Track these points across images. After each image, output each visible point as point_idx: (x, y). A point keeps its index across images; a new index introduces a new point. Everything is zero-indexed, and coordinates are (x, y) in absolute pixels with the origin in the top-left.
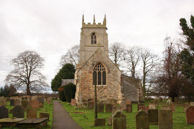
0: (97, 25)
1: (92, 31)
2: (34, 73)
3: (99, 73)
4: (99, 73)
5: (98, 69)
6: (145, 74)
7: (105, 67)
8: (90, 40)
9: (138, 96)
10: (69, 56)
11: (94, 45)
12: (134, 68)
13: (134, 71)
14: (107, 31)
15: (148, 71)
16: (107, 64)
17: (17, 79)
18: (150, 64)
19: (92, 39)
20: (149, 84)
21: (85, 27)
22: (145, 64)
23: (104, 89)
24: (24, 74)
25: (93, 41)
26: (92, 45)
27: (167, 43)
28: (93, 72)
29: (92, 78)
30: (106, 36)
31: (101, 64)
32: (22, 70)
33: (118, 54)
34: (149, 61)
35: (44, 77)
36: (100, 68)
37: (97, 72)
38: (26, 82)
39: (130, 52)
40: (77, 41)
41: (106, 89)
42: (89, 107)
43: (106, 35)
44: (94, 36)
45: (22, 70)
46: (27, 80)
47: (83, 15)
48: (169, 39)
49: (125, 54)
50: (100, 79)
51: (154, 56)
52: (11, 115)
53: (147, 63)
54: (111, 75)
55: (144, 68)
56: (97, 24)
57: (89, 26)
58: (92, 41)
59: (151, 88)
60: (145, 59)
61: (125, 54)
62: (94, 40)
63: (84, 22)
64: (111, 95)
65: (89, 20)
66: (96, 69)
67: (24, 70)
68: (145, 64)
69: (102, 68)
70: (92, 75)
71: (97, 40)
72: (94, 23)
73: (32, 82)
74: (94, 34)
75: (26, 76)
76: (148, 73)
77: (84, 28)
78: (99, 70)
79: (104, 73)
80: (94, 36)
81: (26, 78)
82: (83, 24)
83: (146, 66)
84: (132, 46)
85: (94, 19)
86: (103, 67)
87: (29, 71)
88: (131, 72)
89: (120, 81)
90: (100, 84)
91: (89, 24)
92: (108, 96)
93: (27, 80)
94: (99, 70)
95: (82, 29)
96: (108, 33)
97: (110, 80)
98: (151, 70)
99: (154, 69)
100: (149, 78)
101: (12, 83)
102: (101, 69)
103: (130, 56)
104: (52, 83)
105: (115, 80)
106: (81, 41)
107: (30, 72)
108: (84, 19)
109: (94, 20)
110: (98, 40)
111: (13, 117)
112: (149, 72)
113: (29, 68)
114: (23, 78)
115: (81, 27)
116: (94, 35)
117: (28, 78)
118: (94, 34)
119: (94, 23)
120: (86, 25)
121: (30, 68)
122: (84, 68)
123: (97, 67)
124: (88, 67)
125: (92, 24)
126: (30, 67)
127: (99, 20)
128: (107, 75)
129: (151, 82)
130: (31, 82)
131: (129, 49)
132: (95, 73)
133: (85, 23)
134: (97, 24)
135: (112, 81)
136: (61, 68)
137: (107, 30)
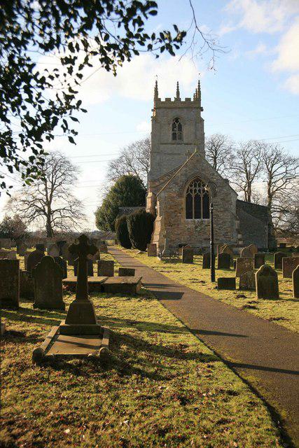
1: (172, 114)
2: (60, 194)
3: (197, 197)
4: (197, 197)
5: (195, 191)
6: (271, 196)
8: (171, 132)
9: (267, 238)
10: (125, 162)
11: (178, 141)
12: (249, 184)
13: (250, 191)
14: (203, 115)
15: (277, 190)
17: (26, 206)
18: (282, 176)
19: (174, 126)
20: (278, 215)
21: (161, 107)
22: (271, 177)
24: (40, 196)
28: (185, 194)
29: (184, 206)
32: (37, 188)
33: (219, 157)
34: (279, 170)
35: (77, 202)
37: (193, 195)
38: (44, 211)
39: (244, 153)
40: (143, 129)
43: (202, 121)
45: (37, 188)
46: (46, 208)
49: (233, 157)
50: (197, 207)
51: (290, 160)
52: (116, 275)
53: (276, 173)
55: (270, 184)
56: (183, 100)
58: (174, 135)
59: (281, 223)
60: (272, 167)
61: (233, 157)
65: (167, 93)
66: (191, 191)
67: (41, 190)
68: (271, 177)
70: (184, 200)
72: (178, 99)
73: (56, 210)
74: (177, 120)
75: (45, 201)
76: (278, 193)
79: (206, 197)
81: (45, 203)
82: (157, 99)
83: (273, 181)
84: (246, 141)
85: (178, 90)
87: (49, 191)
88: (244, 192)
89: (234, 212)
90: (197, 216)
93: (46, 208)
98: (282, 187)
99: (289, 186)
100: (278, 203)
101: (18, 212)
102: (199, 191)
103: (241, 161)
104: (97, 214)
105: (226, 210)
106: (153, 134)
107: (52, 192)
109: (178, 93)
110: (185, 130)
112: (278, 192)
113: (49, 185)
114: (39, 205)
115: (152, 106)
117: (48, 204)
118: (177, 120)
119: (178, 99)
121: (51, 184)
125: (173, 100)
126: (52, 182)
127: (187, 93)
128: (212, 200)
129: (283, 211)
130: (54, 211)
131: (239, 147)
132: (189, 197)
134: (183, 100)
136: (114, 184)
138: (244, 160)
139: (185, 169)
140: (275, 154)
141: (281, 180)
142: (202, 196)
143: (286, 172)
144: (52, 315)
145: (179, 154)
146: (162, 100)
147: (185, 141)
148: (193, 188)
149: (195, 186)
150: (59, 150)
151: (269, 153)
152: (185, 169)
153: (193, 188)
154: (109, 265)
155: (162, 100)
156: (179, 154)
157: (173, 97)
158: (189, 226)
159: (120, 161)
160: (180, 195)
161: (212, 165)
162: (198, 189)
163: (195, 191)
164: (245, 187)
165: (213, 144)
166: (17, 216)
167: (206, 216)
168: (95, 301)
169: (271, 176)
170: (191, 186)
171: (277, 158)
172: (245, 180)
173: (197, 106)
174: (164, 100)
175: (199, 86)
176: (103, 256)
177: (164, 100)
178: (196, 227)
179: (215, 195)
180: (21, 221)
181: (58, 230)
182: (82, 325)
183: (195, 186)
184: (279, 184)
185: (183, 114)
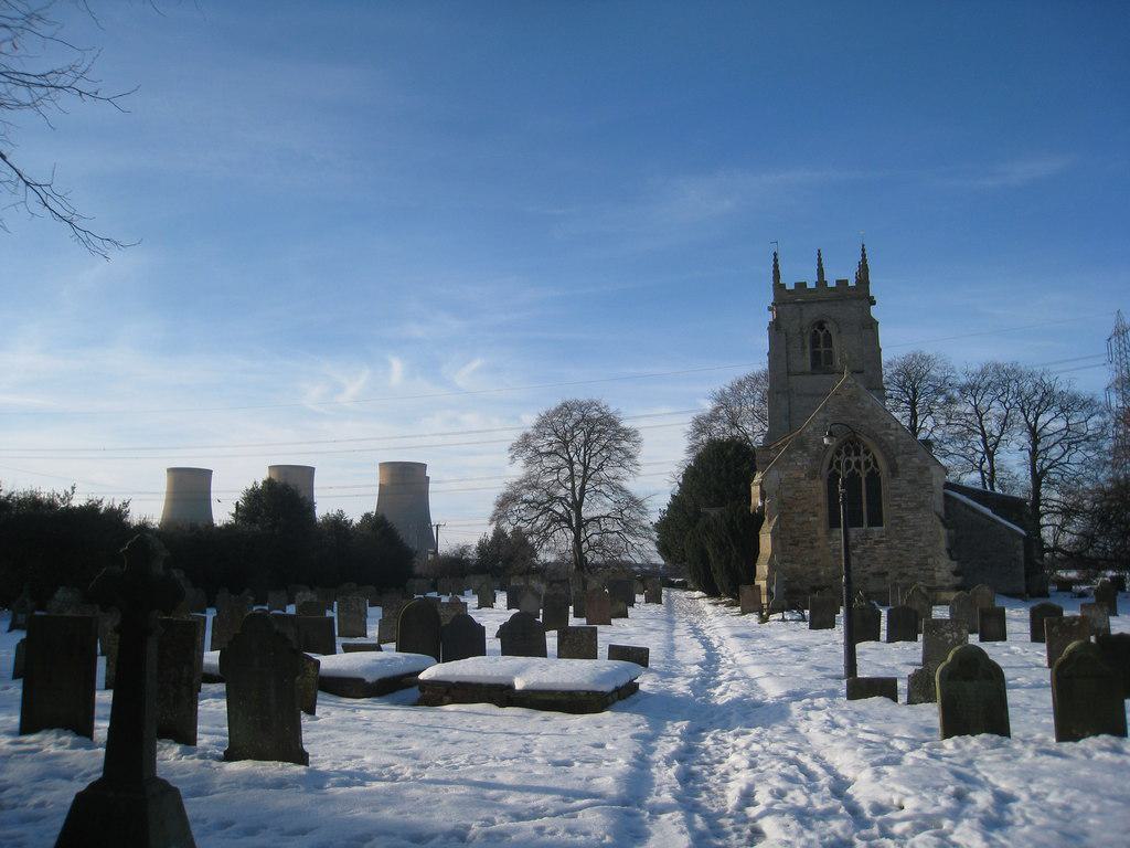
1: (812, 313)
3: (852, 481)
6: (1037, 477)
12: (990, 454)
14: (875, 312)
15: (1050, 467)
16: (885, 438)
18: (1057, 437)
19: (815, 342)
21: (787, 301)
23: (877, 542)
24: (562, 492)
29: (822, 498)
38: (569, 521)
44: (821, 334)
55: (1034, 454)
56: (832, 284)
58: (816, 356)
60: (1036, 419)
62: (822, 349)
64: (905, 570)
65: (798, 273)
66: (838, 463)
72: (821, 282)
74: (821, 325)
79: (874, 478)
82: (778, 286)
83: (1040, 447)
88: (979, 474)
90: (854, 520)
91: (801, 286)
98: (1062, 461)
103: (969, 409)
105: (922, 505)
106: (773, 356)
109: (820, 272)
114: (560, 509)
116: (822, 328)
117: (577, 505)
118: (821, 325)
119: (821, 282)
122: (791, 460)
125: (852, 283)
126: (584, 464)
127: (841, 271)
130: (588, 521)
131: (963, 380)
134: (832, 284)
138: (976, 406)
139: (822, 415)
140: (1040, 391)
141: (1058, 447)
142: (863, 476)
143: (1068, 428)
148: (843, 459)
150: (595, 398)
151: (1028, 386)
152: (822, 415)
153: (843, 459)
154: (586, 636)
159: (714, 417)
160: (813, 475)
161: (905, 423)
162: (853, 459)
163: (848, 464)
164: (982, 463)
165: (908, 375)
166: (517, 532)
167: (876, 520)
168: (683, 724)
169: (1035, 435)
170: (839, 453)
171: (1047, 398)
172: (980, 448)
174: (793, 287)
177: (793, 287)
180: (526, 541)
181: (598, 559)
184: (1055, 452)
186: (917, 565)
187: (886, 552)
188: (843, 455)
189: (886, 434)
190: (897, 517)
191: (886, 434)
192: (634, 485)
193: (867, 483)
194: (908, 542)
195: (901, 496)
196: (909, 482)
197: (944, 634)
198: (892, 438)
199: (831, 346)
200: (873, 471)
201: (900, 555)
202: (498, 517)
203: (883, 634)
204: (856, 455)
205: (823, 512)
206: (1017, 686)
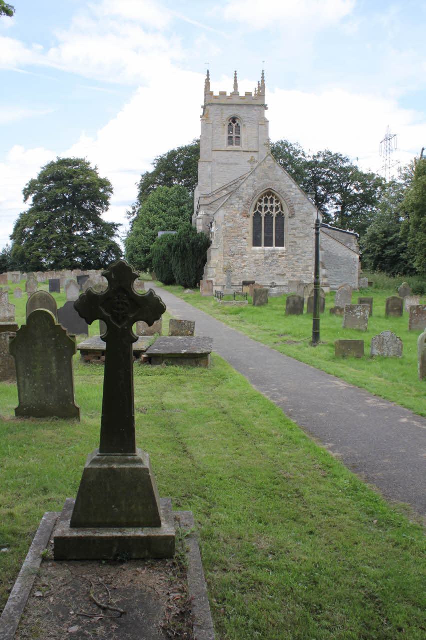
0: (242, 98)
1: (229, 112)
3: (268, 216)
4: (268, 216)
5: (266, 208)
7: (283, 202)
8: (226, 135)
11: (235, 147)
14: (267, 114)
16: (288, 193)
19: (230, 130)
25: (231, 137)
26: (230, 147)
27: (388, 149)
28: (252, 213)
29: (250, 228)
30: (263, 126)
31: (273, 195)
36: (269, 205)
37: (263, 214)
41: (283, 256)
42: (257, 302)
44: (234, 125)
47: (263, 71)
48: (393, 139)
50: (268, 231)
54: (296, 221)
56: (242, 94)
57: (236, 100)
58: (230, 138)
63: (211, 90)
64: (295, 273)
65: (222, 85)
66: (260, 208)
69: (274, 204)
70: (250, 221)
71: (243, 135)
72: (235, 93)
74: (234, 120)
77: (209, 104)
78: (269, 210)
79: (280, 217)
80: (234, 125)
82: (208, 93)
86: (277, 201)
90: (268, 243)
91: (223, 94)
92: (289, 275)
94: (269, 210)
95: (204, 107)
96: (268, 120)
97: (294, 235)
108: (237, 75)
109: (236, 86)
111: (150, 324)
116: (234, 122)
118: (234, 120)
119: (235, 93)
120: (216, 97)
122: (231, 204)
123: (263, 203)
124: (241, 201)
125: (228, 94)
127: (247, 86)
128: (288, 223)
132: (257, 216)
133: (212, 93)
134: (242, 94)
135: (300, 237)
137: (265, 111)
144: (85, 345)
145: (236, 164)
146: (214, 94)
147: (244, 147)
148: (263, 204)
149: (266, 201)
153: (263, 204)
155: (214, 94)
156: (236, 164)
157: (229, 91)
158: (257, 256)
167: (280, 243)
173: (259, 102)
174: (218, 94)
175: (263, 77)
176: (52, 347)
177: (218, 94)
178: (266, 258)
179: (292, 216)
182: (130, 532)
183: (266, 201)
185: (241, 113)
186: (302, 270)
187: (286, 262)
188: (263, 203)
189: (290, 191)
190: (293, 242)
191: (290, 191)
192: (106, 217)
193: (265, 220)
194: (298, 257)
195: (295, 229)
196: (301, 221)
197: (356, 313)
198: (292, 194)
199: (239, 134)
200: (269, 212)
201: (293, 264)
202: (205, 102)
203: (305, 312)
204: (270, 203)
205: (250, 237)
206: (29, 278)
